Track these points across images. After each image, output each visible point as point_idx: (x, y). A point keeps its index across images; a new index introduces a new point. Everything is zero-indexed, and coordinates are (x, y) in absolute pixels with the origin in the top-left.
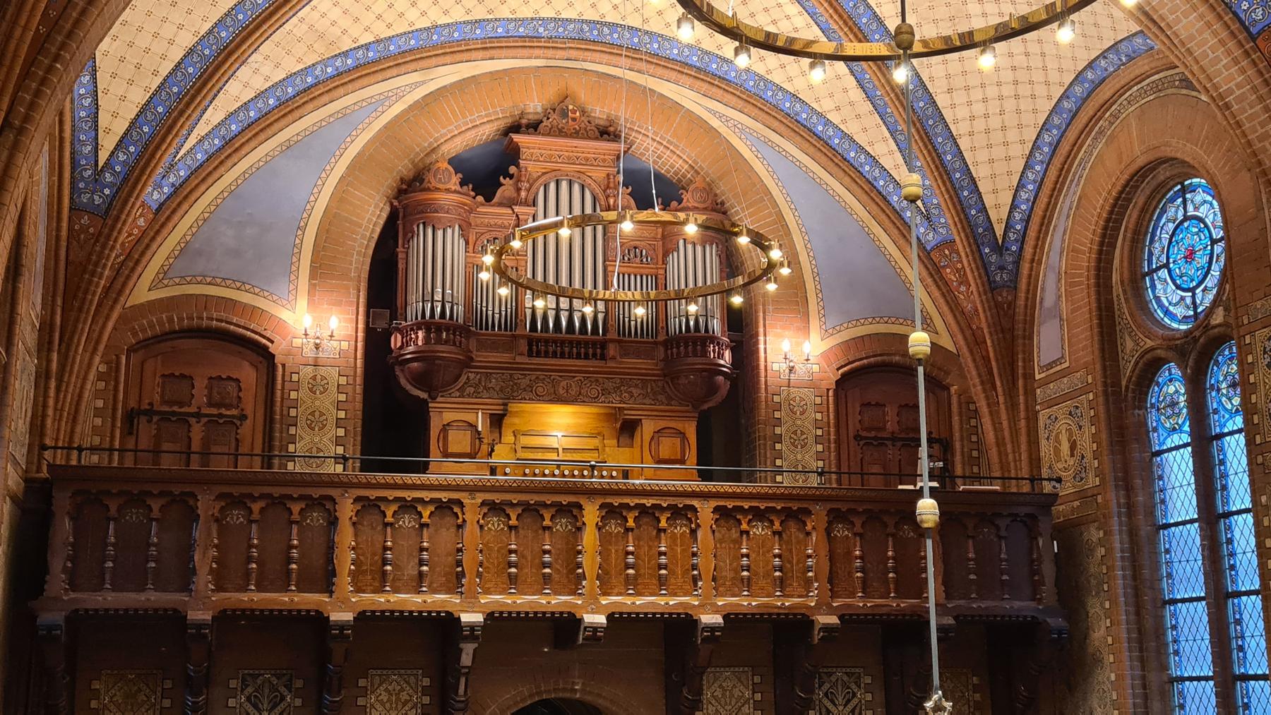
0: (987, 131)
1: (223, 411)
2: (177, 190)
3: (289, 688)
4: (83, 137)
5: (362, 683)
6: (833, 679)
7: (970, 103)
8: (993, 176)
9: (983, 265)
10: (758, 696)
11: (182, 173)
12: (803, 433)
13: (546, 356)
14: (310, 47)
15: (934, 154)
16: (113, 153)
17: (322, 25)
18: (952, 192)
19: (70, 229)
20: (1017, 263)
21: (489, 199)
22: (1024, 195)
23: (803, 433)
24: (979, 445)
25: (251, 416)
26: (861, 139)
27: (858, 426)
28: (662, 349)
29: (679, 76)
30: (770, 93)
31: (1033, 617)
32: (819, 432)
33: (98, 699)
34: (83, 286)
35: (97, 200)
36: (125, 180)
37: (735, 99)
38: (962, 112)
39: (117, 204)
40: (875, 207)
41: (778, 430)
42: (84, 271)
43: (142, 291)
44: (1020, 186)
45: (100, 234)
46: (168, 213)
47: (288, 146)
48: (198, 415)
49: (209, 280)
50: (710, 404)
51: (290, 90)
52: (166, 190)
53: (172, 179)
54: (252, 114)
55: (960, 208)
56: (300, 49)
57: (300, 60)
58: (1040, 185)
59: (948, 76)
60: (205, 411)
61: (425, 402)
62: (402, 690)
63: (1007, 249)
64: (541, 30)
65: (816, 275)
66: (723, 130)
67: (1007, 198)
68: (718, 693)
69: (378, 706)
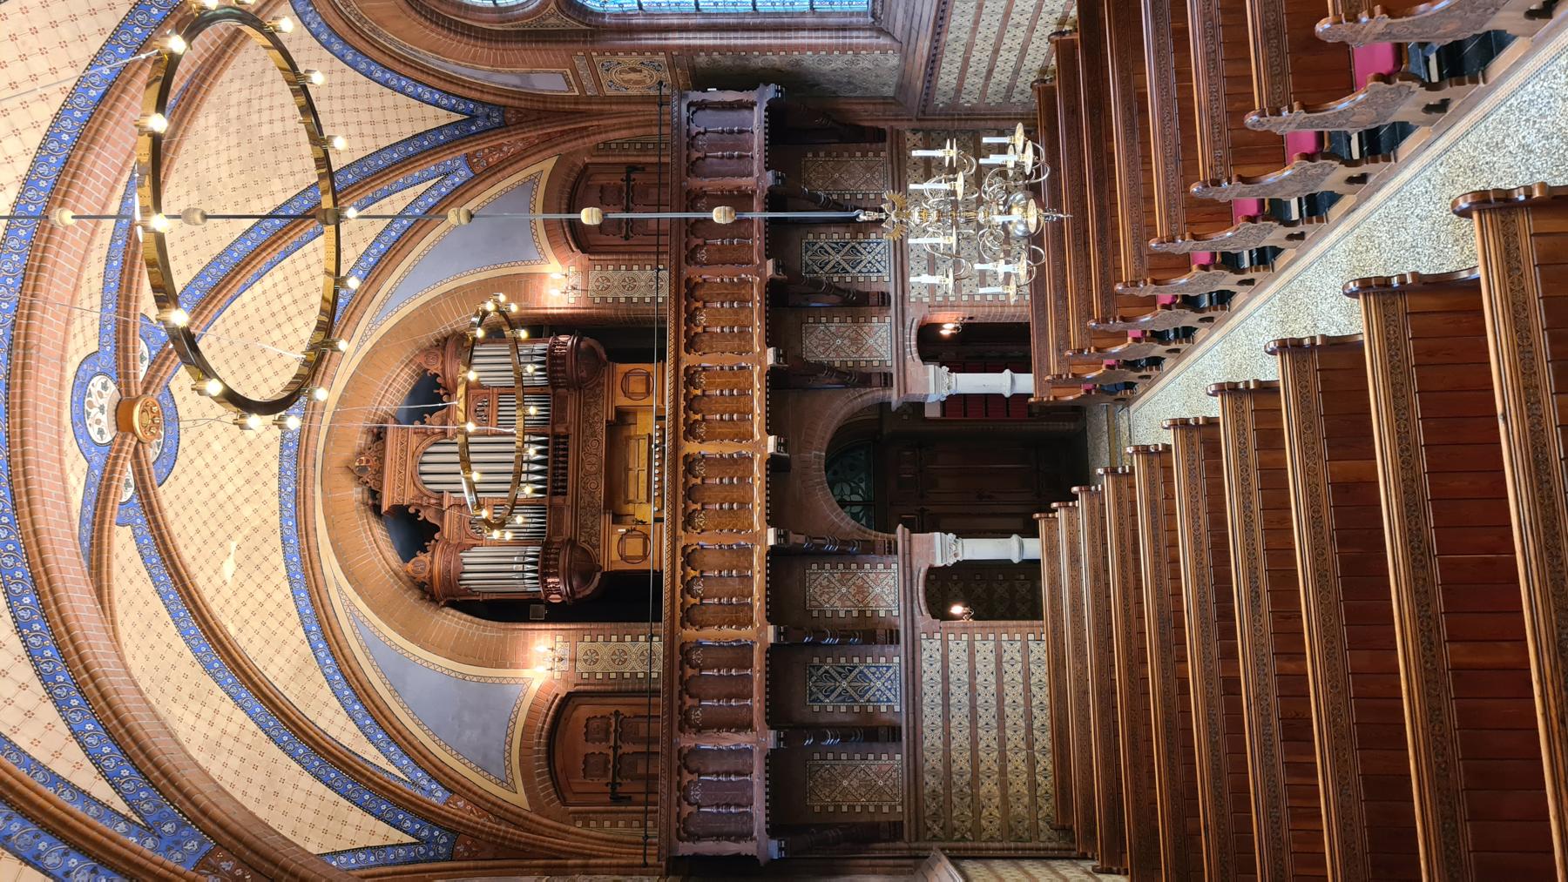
0: (373, 123)
1: (612, 729)
2: (433, 778)
4: (392, 857)
5: (815, 614)
8: (411, 120)
9: (485, 132)
10: (824, 320)
12: (624, 281)
14: (309, 679)
20: (484, 104)
22: (427, 96)
24: (631, 142)
32: (623, 267)
35: (444, 840)
36: (427, 820)
41: (622, 300)
43: (518, 798)
44: (419, 98)
45: (471, 836)
47: (395, 691)
48: (615, 748)
52: (434, 786)
53: (425, 782)
55: (437, 149)
57: (321, 687)
60: (612, 743)
64: (289, 489)
66: (374, 339)
67: (430, 110)
68: (821, 349)
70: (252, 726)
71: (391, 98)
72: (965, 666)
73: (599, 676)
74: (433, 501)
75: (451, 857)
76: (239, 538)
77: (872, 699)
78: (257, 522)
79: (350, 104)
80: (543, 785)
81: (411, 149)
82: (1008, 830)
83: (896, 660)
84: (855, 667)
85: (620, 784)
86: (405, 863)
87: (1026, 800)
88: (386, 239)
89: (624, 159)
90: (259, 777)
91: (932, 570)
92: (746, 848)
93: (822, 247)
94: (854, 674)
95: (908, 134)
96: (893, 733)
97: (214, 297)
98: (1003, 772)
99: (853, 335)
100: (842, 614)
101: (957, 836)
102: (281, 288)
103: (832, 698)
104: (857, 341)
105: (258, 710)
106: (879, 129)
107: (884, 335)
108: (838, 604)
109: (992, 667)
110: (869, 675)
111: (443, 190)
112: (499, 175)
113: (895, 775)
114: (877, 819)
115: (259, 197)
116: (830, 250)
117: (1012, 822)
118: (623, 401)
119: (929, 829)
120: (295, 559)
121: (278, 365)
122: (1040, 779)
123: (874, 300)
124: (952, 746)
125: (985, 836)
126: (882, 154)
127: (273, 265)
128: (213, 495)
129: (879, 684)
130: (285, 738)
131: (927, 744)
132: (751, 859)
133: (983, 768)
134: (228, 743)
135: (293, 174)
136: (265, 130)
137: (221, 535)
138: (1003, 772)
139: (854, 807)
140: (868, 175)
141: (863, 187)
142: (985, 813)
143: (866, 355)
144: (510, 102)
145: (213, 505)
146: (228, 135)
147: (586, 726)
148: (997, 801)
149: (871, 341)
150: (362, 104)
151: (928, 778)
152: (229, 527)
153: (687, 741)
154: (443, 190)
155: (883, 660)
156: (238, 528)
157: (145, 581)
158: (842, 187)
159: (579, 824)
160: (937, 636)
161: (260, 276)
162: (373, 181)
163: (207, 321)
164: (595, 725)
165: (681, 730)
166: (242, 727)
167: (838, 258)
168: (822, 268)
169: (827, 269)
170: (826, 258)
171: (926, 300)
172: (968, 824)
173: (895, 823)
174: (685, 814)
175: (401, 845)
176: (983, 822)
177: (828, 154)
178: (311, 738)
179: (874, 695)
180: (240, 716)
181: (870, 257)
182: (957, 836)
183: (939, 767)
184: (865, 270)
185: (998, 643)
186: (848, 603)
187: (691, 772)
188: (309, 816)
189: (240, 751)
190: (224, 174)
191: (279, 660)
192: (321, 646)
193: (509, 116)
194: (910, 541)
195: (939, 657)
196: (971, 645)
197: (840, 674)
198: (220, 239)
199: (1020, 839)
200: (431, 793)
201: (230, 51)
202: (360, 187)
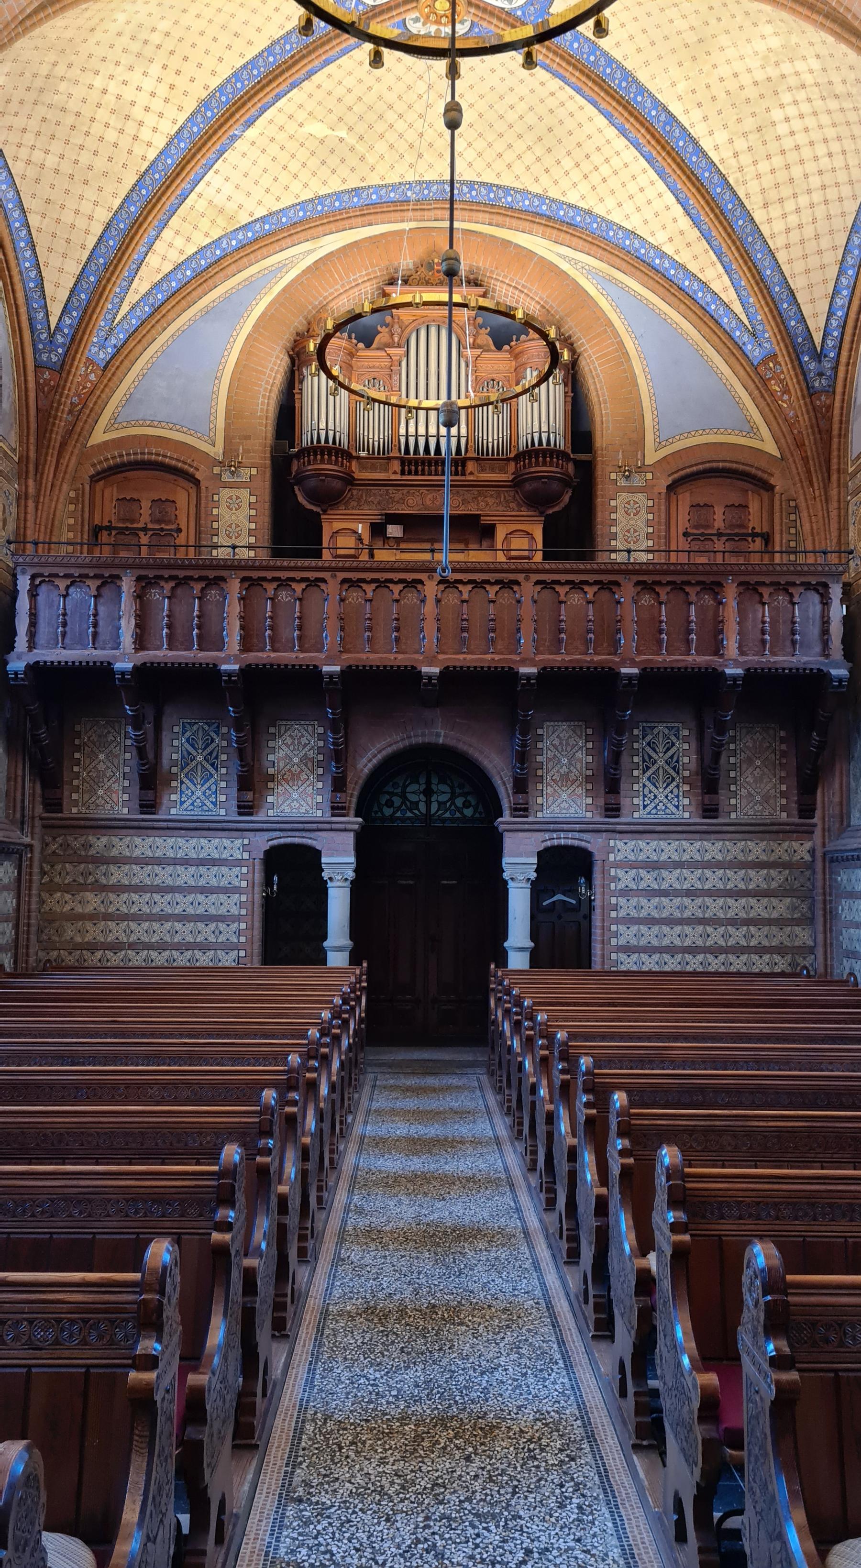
0: (802, 242)
1: (163, 526)
2: (118, 350)
3: (217, 733)
4: (35, 305)
5: (272, 730)
6: (656, 731)
7: (784, 216)
8: (810, 286)
10: (590, 745)
11: (121, 336)
12: (635, 531)
13: (416, 473)
14: (213, 222)
15: (754, 271)
16: (60, 318)
17: (219, 200)
18: (772, 306)
19: (37, 383)
20: (835, 369)
21: (368, 345)
22: (839, 302)
23: (635, 531)
25: (184, 528)
26: (693, 267)
27: (688, 525)
28: (513, 464)
29: (532, 225)
30: (611, 233)
31: (818, 669)
32: (650, 530)
33: (79, 738)
34: (49, 428)
35: (54, 359)
36: (73, 340)
37: (581, 242)
38: (778, 226)
39: (69, 361)
40: (708, 330)
41: (613, 529)
42: (49, 417)
43: (99, 436)
45: (58, 385)
46: (113, 369)
47: (207, 312)
48: (145, 529)
49: (148, 422)
50: (556, 509)
51: (203, 262)
52: (110, 350)
53: (114, 341)
54: (174, 284)
56: (205, 224)
58: (854, 289)
59: (763, 191)
60: (150, 526)
61: (318, 514)
62: (303, 736)
63: (826, 356)
64: (409, 193)
65: (653, 396)
67: (823, 307)
68: (557, 742)
69: (284, 747)
70: (152, 155)
71: (832, 258)
72: (214, 882)
73: (215, 512)
74: (396, 339)
75: (38, 367)
76: (351, 140)
77: (184, 786)
78: (371, 159)
79: (820, 211)
80: (113, 457)
81: (777, 289)
82: (50, 919)
83: (223, 812)
84: (216, 769)
85: (109, 535)
86: (30, 319)
87: (78, 939)
88: (681, 276)
89: (777, 528)
90: (100, 163)
91: (318, 854)
92: (21, 641)
93: (673, 744)
94: (209, 767)
95: (808, 845)
96: (149, 806)
97: (588, 77)
98: (107, 917)
99: (572, 777)
100: (271, 757)
101: (47, 867)
102: (616, 162)
103: (187, 746)
104: (565, 779)
105: (169, 161)
106: (814, 810)
107: (572, 810)
108: (281, 754)
109: (213, 911)
110: (208, 784)
111: (738, 333)
112: (756, 392)
113: (108, 807)
114: (66, 787)
115: (705, 118)
116: (670, 753)
117: (57, 924)
118: (501, 533)
119: (54, 839)
120: (337, 204)
121: (537, 168)
122: (99, 954)
123: (612, 798)
124: (134, 866)
125: (45, 895)
126: (784, 815)
127: (637, 146)
128: (390, 107)
129: (199, 793)
130: (144, 192)
131: (138, 840)
132: (10, 646)
133: (112, 896)
134: (131, 128)
135: (736, 155)
136: (777, 114)
137: (351, 118)
138: (107, 917)
139: (78, 765)
140: (758, 798)
141: (744, 792)
142: (68, 897)
143: (550, 790)
144: (838, 398)
145: (380, 107)
146: (763, 67)
147: (167, 500)
148: (79, 909)
149: (564, 796)
150: (822, 226)
151: (104, 840)
152: (361, 128)
153: (127, 585)
154: (738, 333)
155: (223, 798)
156: (361, 138)
157: (282, 27)
158: (744, 767)
159: (72, 494)
160: (246, 856)
161: (623, 132)
162: (737, 249)
163: (561, 71)
164: (169, 510)
165: (139, 579)
166: (149, 144)
167: (661, 763)
168: (649, 744)
169: (648, 749)
170: (661, 749)
171: (612, 857)
172: (57, 879)
173: (61, 805)
174: (57, 582)
175: (47, 315)
176: (59, 894)
177: (784, 754)
178: (145, 218)
179: (188, 788)
180: (160, 142)
181: (661, 797)
182: (47, 867)
183: (114, 852)
184: (646, 791)
185: (238, 919)
186: (282, 765)
187: (98, 588)
188: (68, 217)
189: (125, 142)
190: (725, 71)
191: (228, 188)
192: (250, 234)
193: (823, 398)
194: (345, 830)
195: (224, 856)
196: (237, 890)
197: (210, 754)
198: (653, 77)
199: (40, 931)
200: (102, 347)
201: (820, 19)
202: (729, 235)
